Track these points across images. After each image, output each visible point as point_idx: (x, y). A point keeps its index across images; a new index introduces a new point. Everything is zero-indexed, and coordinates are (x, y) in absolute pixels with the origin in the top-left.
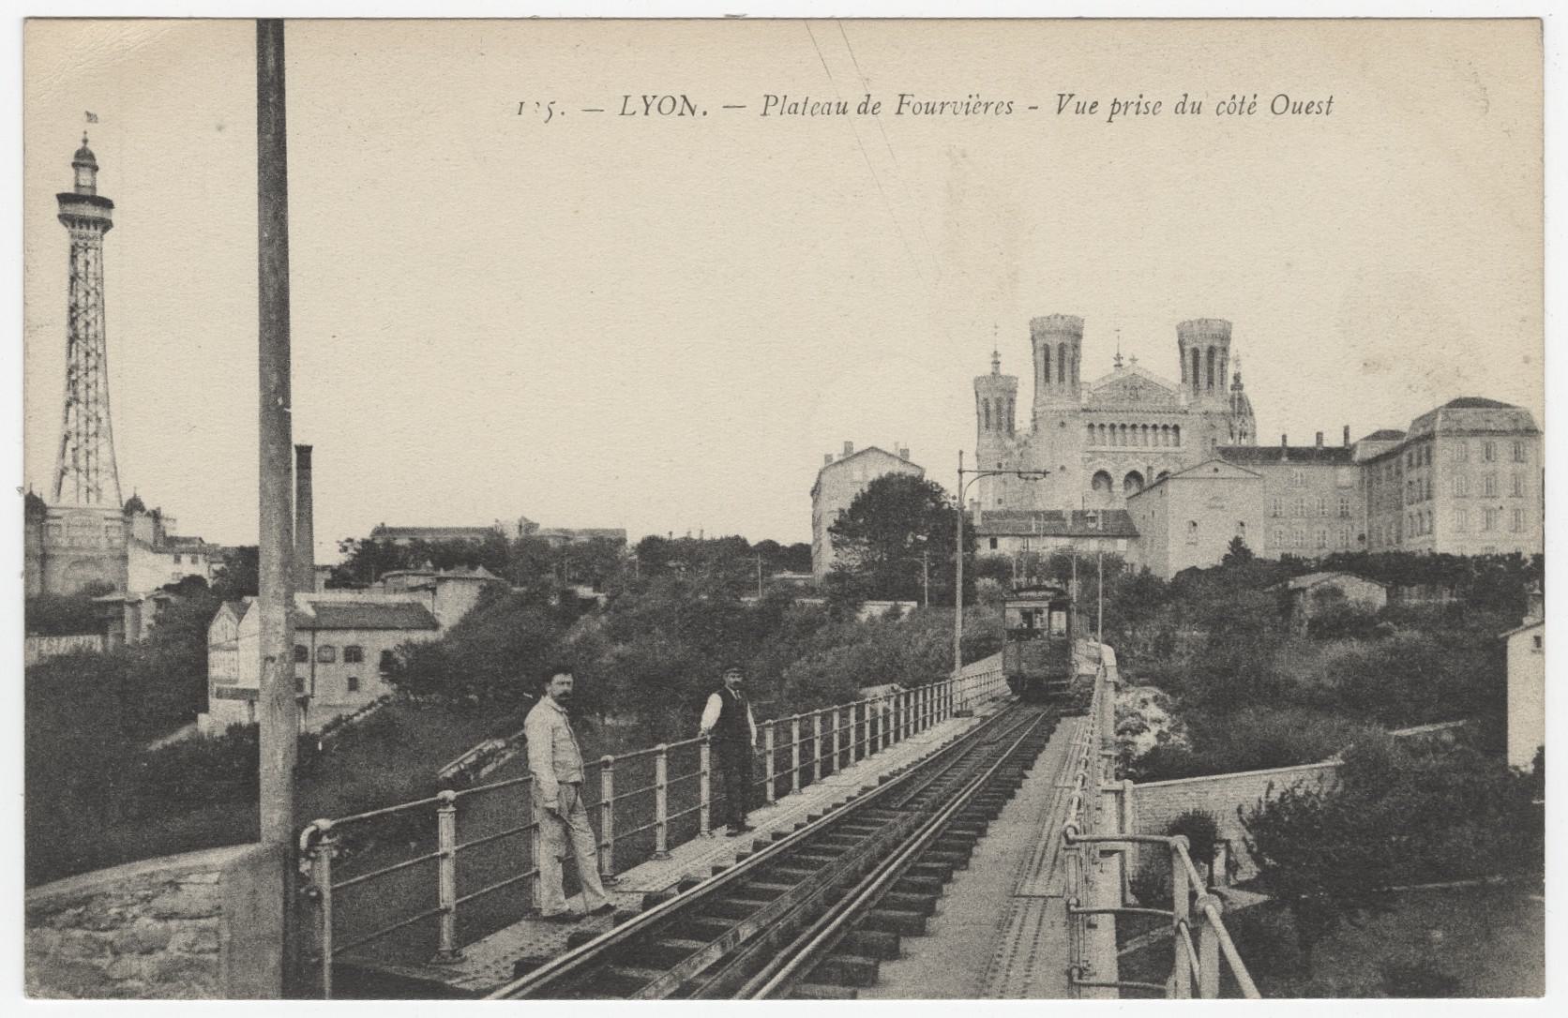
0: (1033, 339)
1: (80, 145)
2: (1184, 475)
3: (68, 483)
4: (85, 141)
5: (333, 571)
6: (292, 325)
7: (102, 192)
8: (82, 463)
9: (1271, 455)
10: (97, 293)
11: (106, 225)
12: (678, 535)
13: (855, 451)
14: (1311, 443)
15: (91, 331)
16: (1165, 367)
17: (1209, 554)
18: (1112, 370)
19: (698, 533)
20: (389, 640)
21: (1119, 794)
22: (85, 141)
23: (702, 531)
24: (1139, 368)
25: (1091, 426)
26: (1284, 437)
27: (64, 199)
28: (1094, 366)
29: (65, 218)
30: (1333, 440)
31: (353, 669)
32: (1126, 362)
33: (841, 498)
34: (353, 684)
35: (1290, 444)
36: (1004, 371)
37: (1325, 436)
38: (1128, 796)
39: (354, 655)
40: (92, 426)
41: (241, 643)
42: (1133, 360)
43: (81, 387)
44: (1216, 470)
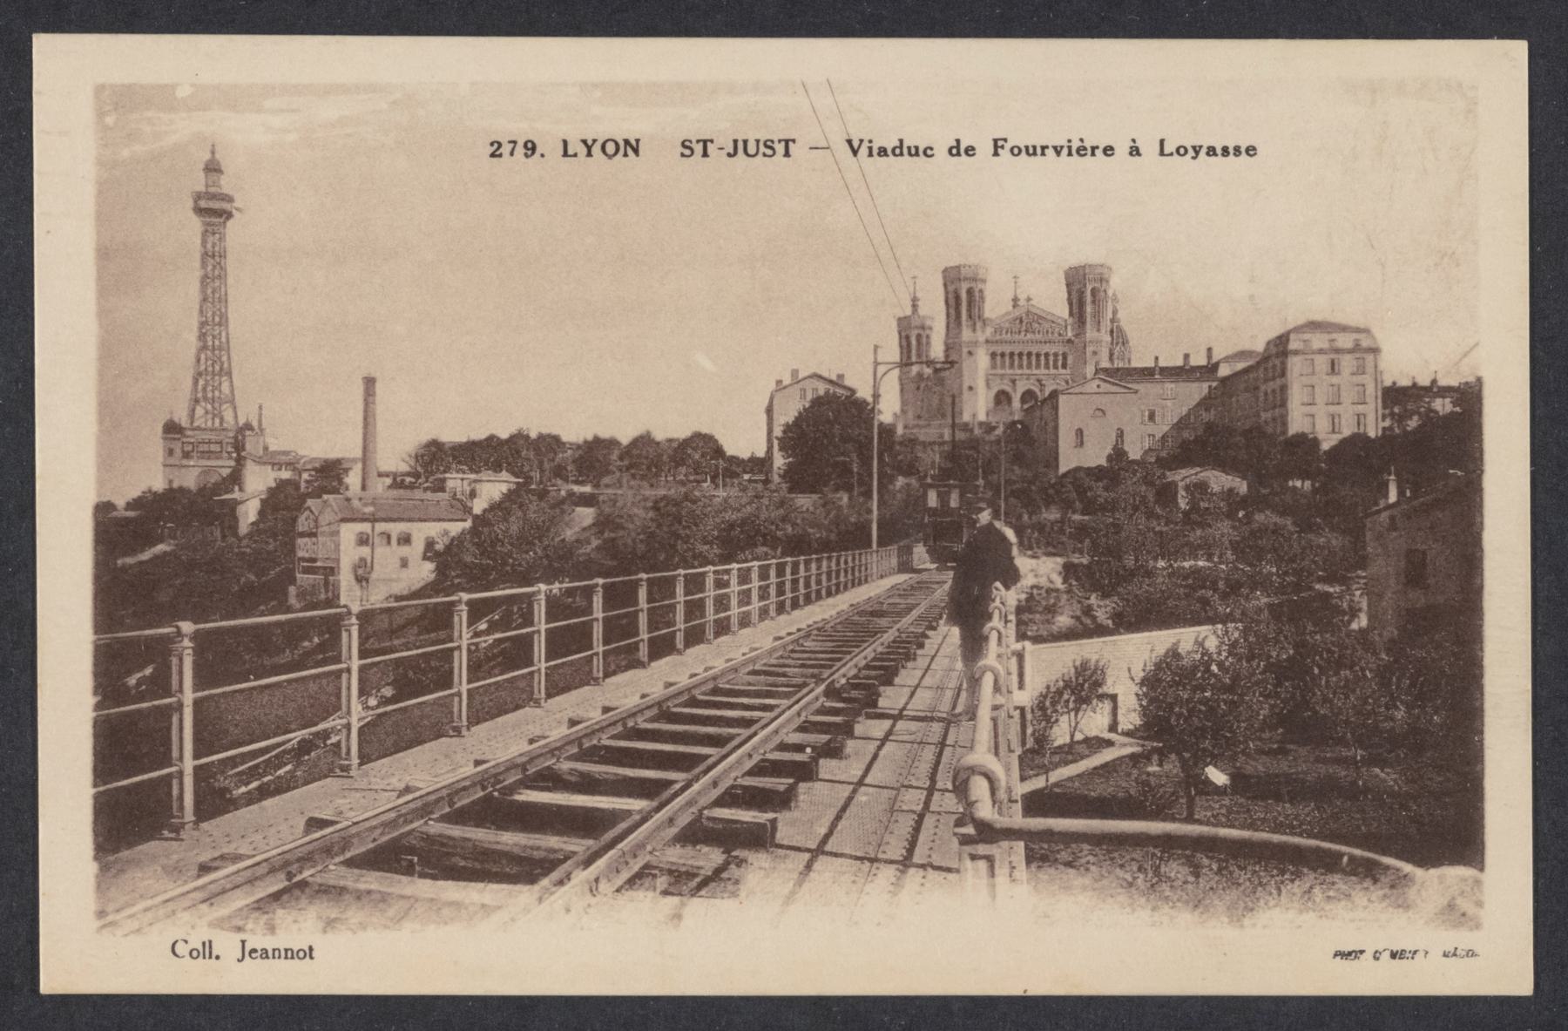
0: (945, 285)
1: (208, 156)
2: (1070, 391)
3: (199, 411)
4: (213, 153)
5: (395, 475)
6: (1532, 924)
7: (226, 190)
8: (210, 395)
9: (1147, 374)
10: (221, 268)
11: (198, 197)
12: (464, 440)
13: (800, 377)
14: (1180, 363)
15: (217, 295)
16: (1054, 302)
17: (1095, 455)
18: (1011, 308)
19: (1204, 353)
20: (433, 529)
21: (1020, 656)
22: (213, 153)
23: (1157, 358)
24: (1032, 305)
25: (993, 355)
26: (1187, 356)
27: (198, 197)
28: (996, 306)
29: (199, 211)
30: (1199, 360)
31: (404, 551)
32: (1022, 303)
33: (788, 412)
34: (404, 563)
35: (1162, 363)
36: (922, 311)
37: (1160, 360)
38: (1028, 658)
39: (406, 540)
40: (217, 368)
41: (320, 530)
42: (1029, 299)
43: (209, 339)
44: (1098, 386)
